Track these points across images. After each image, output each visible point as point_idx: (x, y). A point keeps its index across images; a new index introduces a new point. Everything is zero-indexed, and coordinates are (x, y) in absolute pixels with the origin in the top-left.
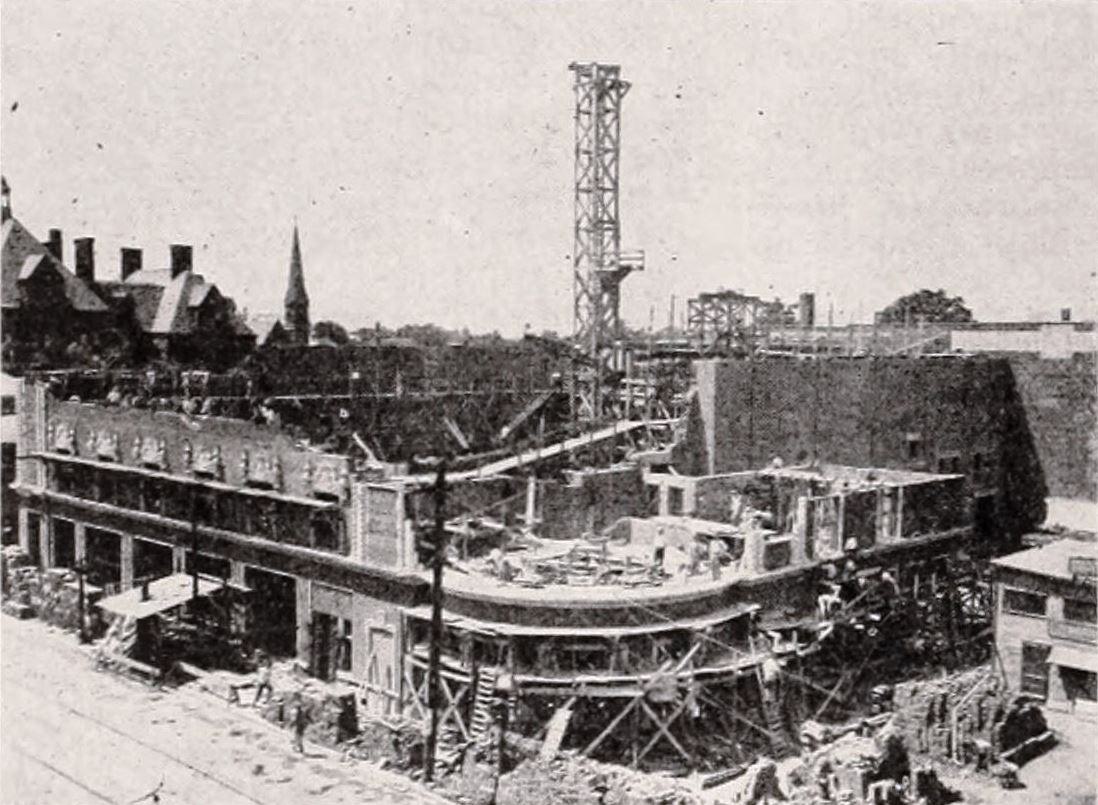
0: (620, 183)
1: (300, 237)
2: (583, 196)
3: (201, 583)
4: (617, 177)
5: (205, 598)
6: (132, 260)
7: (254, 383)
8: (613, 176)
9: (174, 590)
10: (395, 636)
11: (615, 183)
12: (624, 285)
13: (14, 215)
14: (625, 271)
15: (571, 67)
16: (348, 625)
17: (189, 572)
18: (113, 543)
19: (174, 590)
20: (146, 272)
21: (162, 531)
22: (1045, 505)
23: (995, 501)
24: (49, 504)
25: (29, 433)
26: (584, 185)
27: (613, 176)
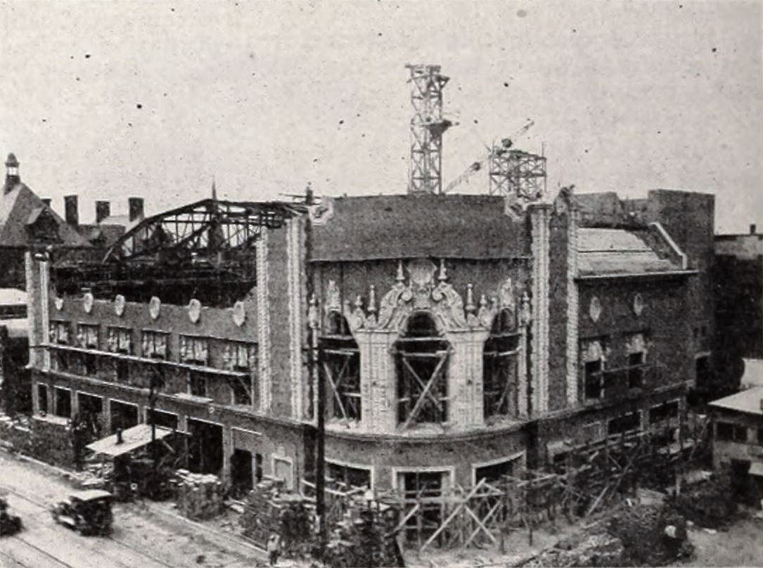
0: (443, 175)
1: (216, 187)
2: (416, 101)
3: (157, 431)
4: (440, 168)
5: (158, 440)
6: (103, 210)
7: (192, 291)
8: (438, 169)
9: (138, 436)
10: (292, 466)
11: (439, 173)
12: (445, 135)
13: (22, 180)
14: (446, 124)
15: (408, 66)
16: (259, 458)
17: (149, 423)
18: (97, 405)
19: (138, 436)
20: (113, 217)
21: (130, 395)
22: (743, 362)
23: (709, 361)
24: (51, 378)
25: (38, 330)
26: (417, 93)
27: (438, 169)
